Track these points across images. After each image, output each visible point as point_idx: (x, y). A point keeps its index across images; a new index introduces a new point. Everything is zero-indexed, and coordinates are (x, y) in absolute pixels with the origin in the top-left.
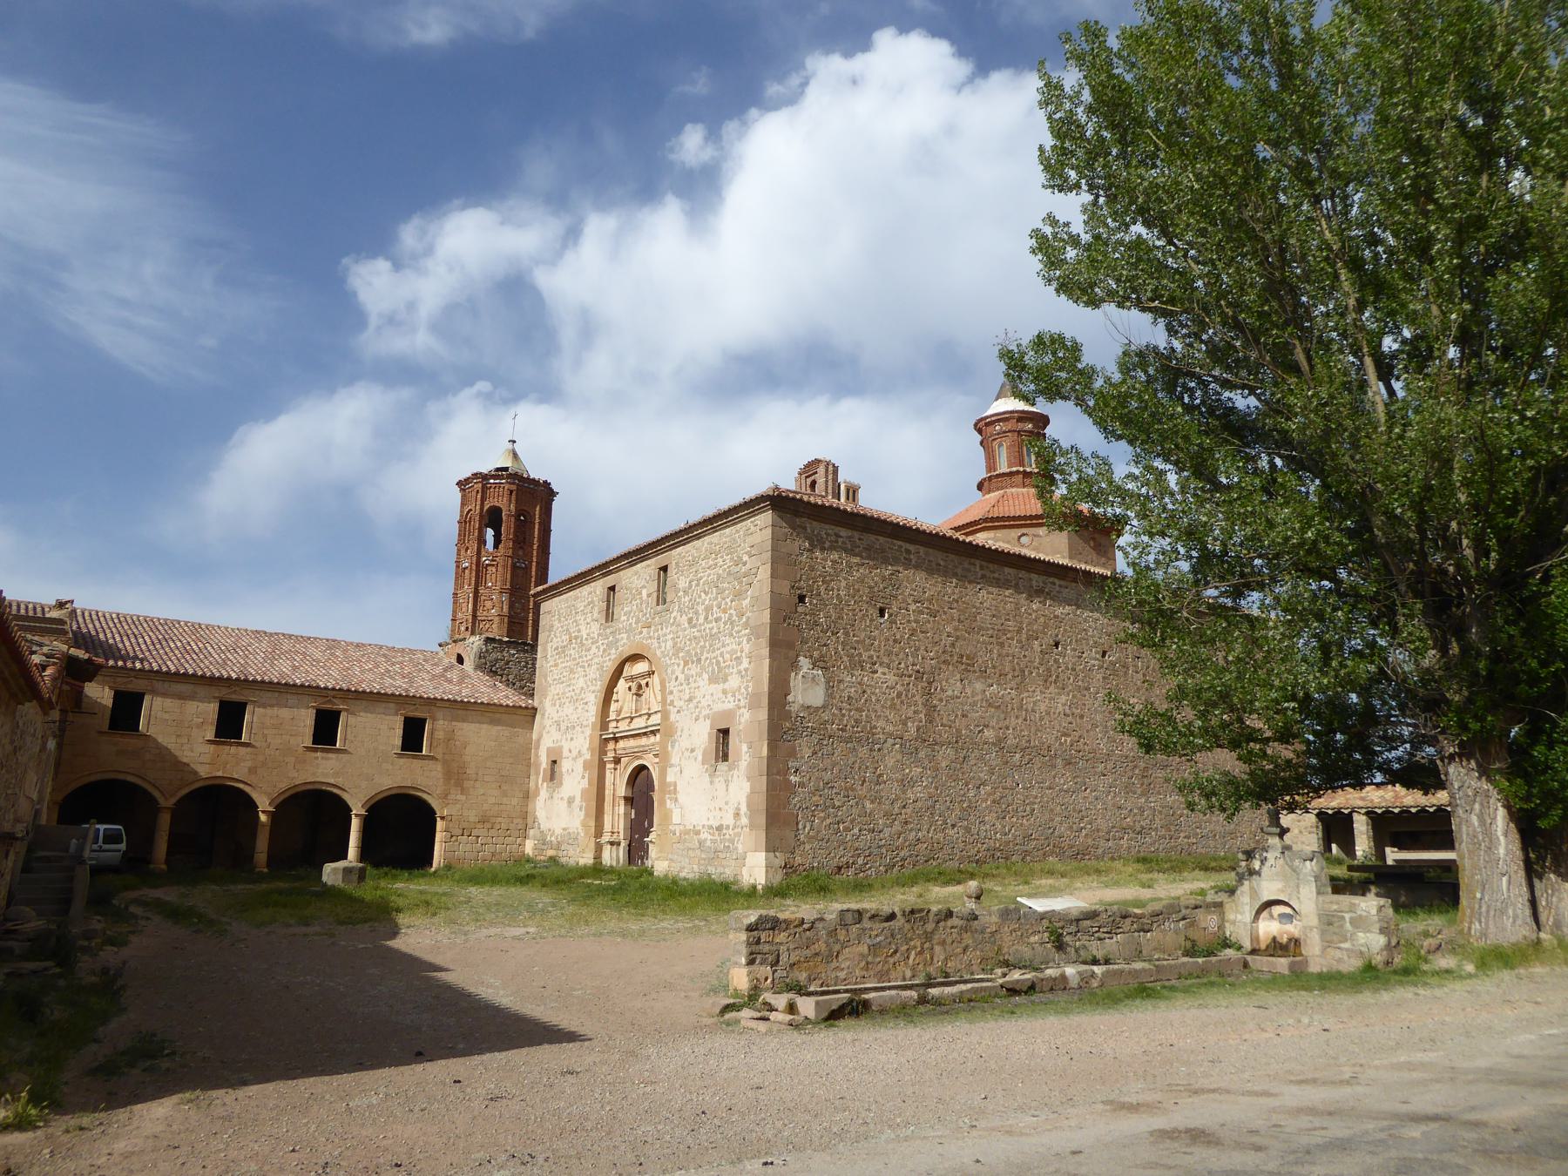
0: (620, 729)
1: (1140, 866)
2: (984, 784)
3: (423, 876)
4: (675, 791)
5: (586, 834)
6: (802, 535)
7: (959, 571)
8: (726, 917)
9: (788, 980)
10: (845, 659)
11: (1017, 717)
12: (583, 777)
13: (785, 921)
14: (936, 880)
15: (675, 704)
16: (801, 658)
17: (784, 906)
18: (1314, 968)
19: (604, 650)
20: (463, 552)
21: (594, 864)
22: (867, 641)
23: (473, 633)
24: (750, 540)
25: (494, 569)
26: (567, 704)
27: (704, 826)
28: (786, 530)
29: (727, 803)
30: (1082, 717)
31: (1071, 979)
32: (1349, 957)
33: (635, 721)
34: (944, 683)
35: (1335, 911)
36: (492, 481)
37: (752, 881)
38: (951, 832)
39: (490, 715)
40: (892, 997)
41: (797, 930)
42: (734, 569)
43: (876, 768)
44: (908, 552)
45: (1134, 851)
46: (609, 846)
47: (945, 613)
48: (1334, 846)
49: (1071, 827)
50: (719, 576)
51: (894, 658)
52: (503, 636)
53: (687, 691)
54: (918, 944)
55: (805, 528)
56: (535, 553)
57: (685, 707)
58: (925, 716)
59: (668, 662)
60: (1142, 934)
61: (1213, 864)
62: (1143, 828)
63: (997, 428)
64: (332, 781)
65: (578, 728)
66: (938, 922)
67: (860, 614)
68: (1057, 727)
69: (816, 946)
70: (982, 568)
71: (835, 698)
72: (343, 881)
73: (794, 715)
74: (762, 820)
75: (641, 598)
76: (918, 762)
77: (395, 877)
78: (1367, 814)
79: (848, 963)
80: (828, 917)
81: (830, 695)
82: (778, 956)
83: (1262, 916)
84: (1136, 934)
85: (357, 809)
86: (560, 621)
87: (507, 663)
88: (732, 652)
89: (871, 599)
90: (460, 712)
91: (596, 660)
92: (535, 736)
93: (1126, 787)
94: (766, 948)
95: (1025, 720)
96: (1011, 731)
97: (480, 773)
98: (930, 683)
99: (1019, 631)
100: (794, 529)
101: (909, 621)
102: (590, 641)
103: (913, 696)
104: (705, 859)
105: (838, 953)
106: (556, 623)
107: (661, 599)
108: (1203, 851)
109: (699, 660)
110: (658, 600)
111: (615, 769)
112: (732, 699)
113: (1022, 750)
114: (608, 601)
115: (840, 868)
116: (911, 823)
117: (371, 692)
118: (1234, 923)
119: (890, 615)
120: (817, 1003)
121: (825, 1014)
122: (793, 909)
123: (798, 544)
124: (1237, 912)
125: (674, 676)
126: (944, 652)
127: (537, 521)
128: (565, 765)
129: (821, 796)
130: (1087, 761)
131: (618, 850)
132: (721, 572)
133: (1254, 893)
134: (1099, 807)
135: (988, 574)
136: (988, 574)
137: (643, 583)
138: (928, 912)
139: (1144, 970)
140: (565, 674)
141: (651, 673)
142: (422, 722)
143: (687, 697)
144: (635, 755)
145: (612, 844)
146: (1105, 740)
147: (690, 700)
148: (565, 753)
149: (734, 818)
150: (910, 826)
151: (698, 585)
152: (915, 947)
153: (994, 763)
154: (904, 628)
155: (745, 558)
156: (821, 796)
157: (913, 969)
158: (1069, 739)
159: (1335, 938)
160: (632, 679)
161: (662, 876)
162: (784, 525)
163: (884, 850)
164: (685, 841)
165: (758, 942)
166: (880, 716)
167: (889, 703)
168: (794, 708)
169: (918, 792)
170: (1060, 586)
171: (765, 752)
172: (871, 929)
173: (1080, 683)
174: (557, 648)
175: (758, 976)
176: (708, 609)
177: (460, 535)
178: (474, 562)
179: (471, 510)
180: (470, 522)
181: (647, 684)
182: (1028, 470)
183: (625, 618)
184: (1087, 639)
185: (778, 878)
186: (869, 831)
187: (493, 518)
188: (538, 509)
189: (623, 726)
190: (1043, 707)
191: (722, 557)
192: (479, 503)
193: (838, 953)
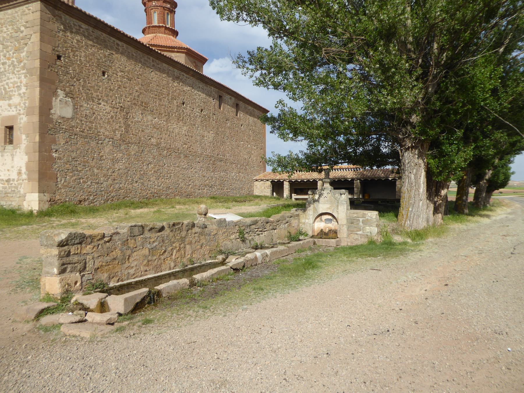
1: (212, 200)
2: (150, 163)
6: (59, 21)
7: (142, 60)
8: (15, 229)
9: (93, 281)
10: (84, 95)
11: (166, 134)
13: (90, 236)
14: (130, 206)
16: (59, 90)
17: (51, 221)
18: (344, 244)
22: (96, 87)
24: (25, 18)
28: (49, 16)
29: (12, 167)
30: (192, 137)
31: (259, 258)
32: (361, 238)
34: (134, 114)
35: (355, 217)
37: (30, 209)
38: (135, 185)
40: (175, 286)
41: (100, 242)
42: (15, 35)
43: (100, 153)
44: (118, 45)
45: (208, 194)
47: (135, 80)
48: (274, 193)
49: (186, 184)
51: (109, 98)
54: (178, 245)
55: (61, 18)
58: (125, 129)
60: (273, 231)
61: (239, 200)
62: (212, 185)
63: (154, 3)
66: (188, 231)
67: (92, 72)
68: (182, 141)
69: (114, 253)
70: (153, 61)
71: (78, 114)
73: (54, 121)
74: (36, 176)
76: (120, 151)
78: (289, 181)
79: (135, 263)
80: (122, 231)
82: (85, 263)
83: (317, 220)
84: (271, 231)
88: (14, 83)
89: (98, 65)
93: (207, 168)
94: (76, 259)
95: (169, 136)
96: (163, 140)
98: (127, 113)
99: (168, 95)
100: (55, 16)
101: (117, 81)
103: (119, 119)
105: (129, 256)
108: (232, 194)
112: (15, 110)
113: (167, 149)
115: (80, 201)
116: (117, 180)
118: (304, 223)
119: (108, 76)
120: (126, 300)
121: (131, 307)
122: (57, 222)
123: (56, 26)
124: (306, 218)
126: (134, 99)
129: (70, 165)
130: (193, 156)
132: (5, 35)
133: (315, 209)
134: (197, 176)
135: (156, 65)
136: (156, 65)
138: (182, 224)
139: (284, 250)
146: (200, 148)
150: (116, 181)
152: (176, 247)
153: (155, 154)
154: (115, 84)
155: (22, 28)
156: (70, 165)
157: (175, 262)
158: (186, 146)
159: (355, 229)
162: (48, 12)
163: (103, 193)
165: (68, 255)
166: (102, 127)
167: (107, 121)
168: (55, 117)
169: (120, 166)
170: (186, 77)
171: (37, 139)
172: (150, 238)
173: (192, 122)
175: (69, 282)
182: (167, 26)
184: (196, 103)
185: (46, 207)
186: (96, 183)
190: (177, 131)
191: (6, 27)
193: (129, 256)
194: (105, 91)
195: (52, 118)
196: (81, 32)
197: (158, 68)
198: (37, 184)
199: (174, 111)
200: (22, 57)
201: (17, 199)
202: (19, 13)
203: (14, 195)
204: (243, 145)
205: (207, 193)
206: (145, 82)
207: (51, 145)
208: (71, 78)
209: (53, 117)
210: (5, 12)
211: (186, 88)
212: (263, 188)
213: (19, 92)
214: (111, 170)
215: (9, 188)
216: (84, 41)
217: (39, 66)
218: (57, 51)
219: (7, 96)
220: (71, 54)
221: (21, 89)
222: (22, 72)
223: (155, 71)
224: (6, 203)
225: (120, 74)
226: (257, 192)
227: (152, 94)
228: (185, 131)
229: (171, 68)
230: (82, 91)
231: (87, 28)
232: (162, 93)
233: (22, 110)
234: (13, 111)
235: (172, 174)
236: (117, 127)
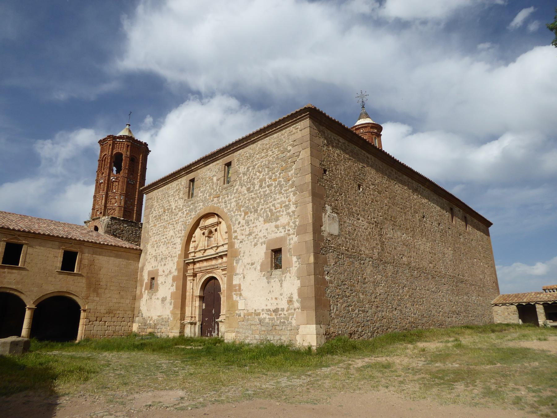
0: (197, 257)
3: (72, 345)
4: (240, 289)
5: (174, 318)
6: (323, 136)
7: (387, 172)
10: (346, 210)
12: (172, 286)
15: (238, 237)
16: (327, 205)
19: (187, 214)
20: (100, 175)
21: (180, 336)
22: (354, 202)
23: (104, 215)
24: (292, 138)
25: (117, 183)
26: (162, 245)
27: (263, 310)
29: (281, 295)
33: (207, 251)
36: (118, 140)
38: (395, 313)
39: (116, 252)
44: (368, 158)
46: (189, 326)
49: (437, 311)
50: (269, 162)
52: (121, 217)
53: (248, 229)
55: (324, 133)
56: (139, 177)
57: (246, 239)
58: (381, 246)
59: (233, 214)
64: (14, 287)
65: (169, 258)
67: (350, 186)
68: (428, 259)
72: (10, 352)
73: (325, 239)
74: (313, 303)
75: (213, 182)
77: (52, 348)
78: (543, 304)
81: (341, 229)
85: (30, 304)
86: (157, 202)
87: (122, 231)
90: (98, 250)
91: (182, 220)
92: (140, 265)
96: (412, 259)
97: (108, 285)
102: (177, 210)
103: (375, 235)
104: (264, 331)
106: (155, 204)
107: (227, 180)
109: (256, 211)
110: (224, 182)
111: (193, 280)
114: (190, 187)
115: (351, 334)
116: (379, 307)
117: (44, 234)
119: (363, 189)
123: (322, 141)
125: (237, 222)
126: (385, 213)
127: (140, 162)
128: (160, 280)
129: (340, 289)
131: (195, 327)
132: (271, 158)
137: (214, 173)
140: (160, 230)
141: (219, 223)
142: (75, 254)
143: (247, 233)
144: (207, 271)
145: (191, 324)
147: (250, 234)
148: (160, 273)
149: (288, 303)
150: (379, 309)
151: (254, 168)
154: (369, 198)
156: (340, 289)
160: (205, 228)
161: (230, 342)
162: (315, 128)
163: (369, 323)
164: (248, 320)
168: (325, 234)
169: (380, 290)
171: (312, 259)
174: (156, 217)
176: (261, 181)
177: (99, 167)
178: (107, 179)
179: (106, 154)
180: (105, 161)
181: (216, 230)
183: (202, 194)
187: (117, 160)
188: (141, 156)
189: (199, 255)
191: (272, 150)
192: (110, 150)
194: (362, 205)
195: (323, 236)
196: (340, 145)
197: (400, 180)
198: (313, 313)
199: (418, 225)
200: (290, 175)
201: (288, 333)
202: (286, 134)
203: (284, 328)
204: (476, 262)
205: (455, 322)
206: (392, 195)
207: (323, 266)
208: (335, 192)
209: (324, 234)
210: (271, 137)
211: (425, 201)
212: (506, 314)
213: (288, 211)
214: (373, 296)
215: (277, 320)
216: (344, 156)
217: (310, 181)
218: (324, 165)
219: (273, 217)
220: (334, 168)
221: (290, 208)
222: (290, 190)
223: (398, 183)
224: (274, 337)
225: (372, 187)
226: (498, 320)
227: (398, 208)
228: (429, 248)
229: (410, 180)
230: (344, 206)
231: (344, 142)
232: (406, 206)
233: (291, 230)
234: (281, 232)
235: (424, 299)
236: (375, 245)
